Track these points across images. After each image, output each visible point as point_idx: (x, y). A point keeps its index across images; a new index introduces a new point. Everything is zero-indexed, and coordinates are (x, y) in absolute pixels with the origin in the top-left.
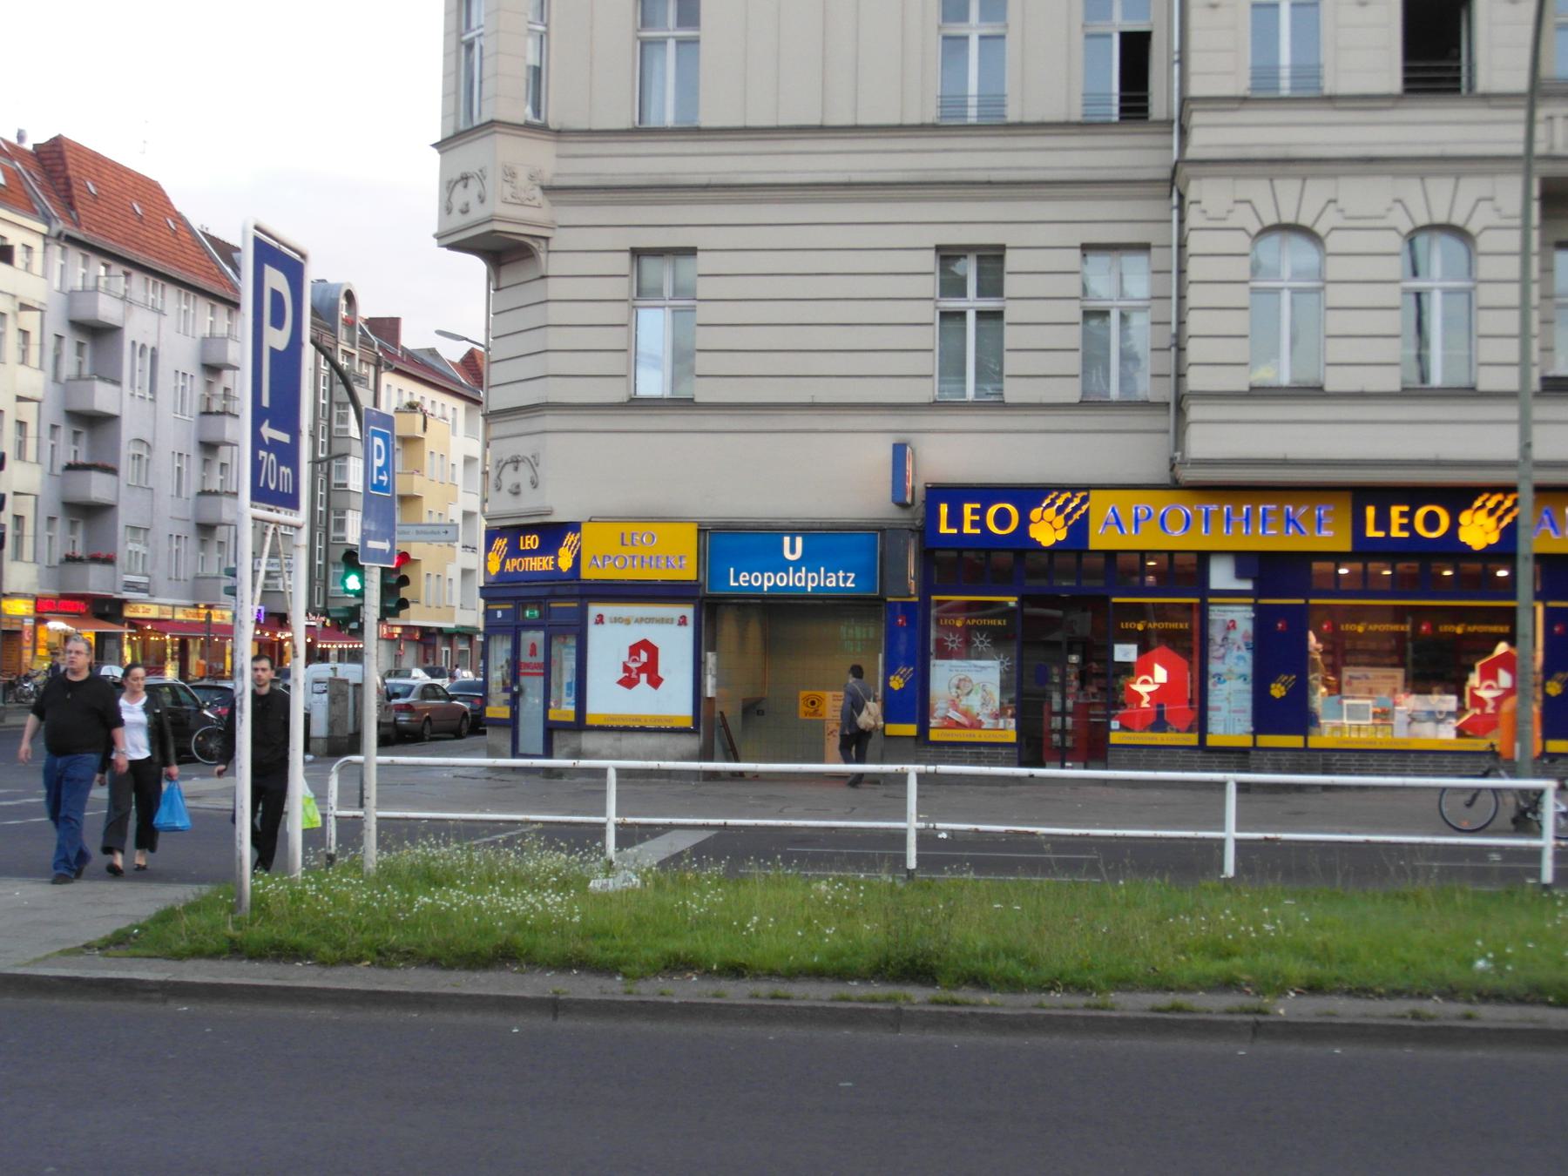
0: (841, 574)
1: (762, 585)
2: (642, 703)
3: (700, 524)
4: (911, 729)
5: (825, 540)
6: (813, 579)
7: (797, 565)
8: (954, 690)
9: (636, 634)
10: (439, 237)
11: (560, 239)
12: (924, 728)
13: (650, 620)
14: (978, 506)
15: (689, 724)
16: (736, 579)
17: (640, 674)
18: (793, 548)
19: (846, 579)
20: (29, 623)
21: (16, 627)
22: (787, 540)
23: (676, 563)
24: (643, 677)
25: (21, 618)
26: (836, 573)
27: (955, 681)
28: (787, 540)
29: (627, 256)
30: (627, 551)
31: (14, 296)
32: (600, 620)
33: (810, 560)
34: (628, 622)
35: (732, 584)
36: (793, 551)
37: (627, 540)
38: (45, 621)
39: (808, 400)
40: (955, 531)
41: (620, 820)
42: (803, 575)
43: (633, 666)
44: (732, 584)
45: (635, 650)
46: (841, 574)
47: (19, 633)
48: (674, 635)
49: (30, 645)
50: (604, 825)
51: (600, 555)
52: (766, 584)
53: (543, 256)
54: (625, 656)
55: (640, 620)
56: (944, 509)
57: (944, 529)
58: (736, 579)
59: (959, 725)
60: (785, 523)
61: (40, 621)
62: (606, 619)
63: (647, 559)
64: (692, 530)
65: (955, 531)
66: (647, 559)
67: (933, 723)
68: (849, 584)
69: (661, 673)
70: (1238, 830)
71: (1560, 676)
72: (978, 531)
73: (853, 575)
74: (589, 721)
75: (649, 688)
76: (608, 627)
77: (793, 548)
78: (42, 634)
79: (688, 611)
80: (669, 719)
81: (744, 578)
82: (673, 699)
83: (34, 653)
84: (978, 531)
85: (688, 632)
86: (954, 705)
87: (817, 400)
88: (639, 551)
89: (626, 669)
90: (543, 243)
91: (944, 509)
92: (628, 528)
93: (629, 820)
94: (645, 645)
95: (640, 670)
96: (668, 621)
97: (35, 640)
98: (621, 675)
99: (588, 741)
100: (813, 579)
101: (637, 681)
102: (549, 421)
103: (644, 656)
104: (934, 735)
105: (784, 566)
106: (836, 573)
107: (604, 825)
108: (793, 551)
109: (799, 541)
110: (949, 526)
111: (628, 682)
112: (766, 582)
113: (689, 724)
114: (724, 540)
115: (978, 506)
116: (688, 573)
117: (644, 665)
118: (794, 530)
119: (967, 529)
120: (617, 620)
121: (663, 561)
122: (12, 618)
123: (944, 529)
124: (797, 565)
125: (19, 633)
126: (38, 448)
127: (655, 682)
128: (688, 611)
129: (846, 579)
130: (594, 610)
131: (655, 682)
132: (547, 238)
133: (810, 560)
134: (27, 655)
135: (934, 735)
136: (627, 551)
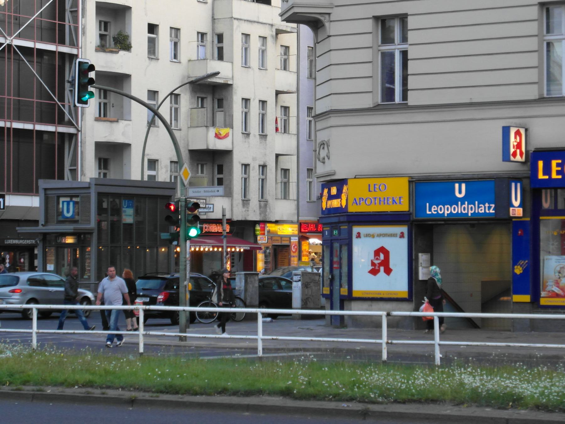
0: (487, 205)
1: (444, 213)
2: (382, 284)
3: (412, 177)
4: (526, 298)
5: (478, 184)
6: (464, 208)
7: (462, 200)
8: (557, 274)
9: (378, 243)
10: (281, 15)
11: (337, 14)
12: (536, 297)
13: (385, 235)
14: (560, 161)
15: (406, 296)
16: (430, 210)
17: (380, 267)
18: (460, 191)
19: (489, 208)
20: (295, 240)
21: (285, 243)
22: (457, 185)
23: (397, 200)
24: (382, 269)
25: (289, 237)
26: (484, 204)
27: (558, 269)
28: (457, 185)
29: (371, 21)
30: (372, 195)
31: (272, 25)
32: (359, 235)
33: (469, 198)
34: (373, 236)
35: (428, 212)
36: (460, 192)
37: (372, 189)
38: (307, 238)
39: (467, 101)
40: (547, 177)
41: (37, 331)
42: (466, 206)
43: (377, 262)
44: (428, 212)
45: (377, 253)
46: (487, 205)
47: (288, 247)
48: (397, 244)
49: (296, 254)
50: (31, 333)
51: (354, 199)
52: (446, 212)
53: (327, 24)
54: (372, 256)
55: (380, 235)
56: (541, 164)
57: (541, 176)
58: (430, 210)
59: (557, 296)
60: (459, 175)
61: (303, 238)
62: (362, 235)
63: (382, 199)
64: (404, 183)
65: (547, 177)
66: (382, 199)
67: (543, 294)
68: (492, 211)
69: (391, 266)
70: (263, 335)
71: (521, 262)
72: (560, 177)
73: (493, 206)
74: (355, 295)
75: (385, 275)
76: (363, 239)
77: (460, 191)
78: (305, 247)
79: (404, 229)
80: (396, 293)
81: (434, 208)
82: (397, 282)
83: (300, 258)
84: (560, 177)
85: (404, 242)
86: (557, 283)
87: (474, 101)
88: (378, 194)
89: (373, 264)
90: (327, 16)
91: (541, 164)
92: (372, 182)
93: (41, 331)
94: (382, 250)
95: (380, 264)
96: (394, 235)
97: (300, 251)
98: (370, 268)
99: (354, 304)
100: (464, 208)
101: (378, 271)
102: (334, 120)
103: (382, 256)
104: (543, 302)
105: (454, 201)
106: (484, 204)
107: (31, 333)
108: (460, 192)
109: (463, 186)
110: (544, 174)
111: (374, 272)
112: (446, 211)
113: (406, 296)
114: (424, 187)
115: (560, 161)
116: (404, 207)
117: (382, 262)
118: (460, 180)
119: (554, 176)
120: (367, 235)
121: (391, 200)
122: (282, 237)
123: (541, 176)
124: (462, 200)
125: (288, 247)
126: (298, 124)
127: (388, 271)
128: (404, 229)
129: (489, 208)
130: (356, 229)
131: (388, 271)
132: (329, 14)
133: (469, 198)
134: (294, 261)
135: (543, 302)
136: (372, 195)
